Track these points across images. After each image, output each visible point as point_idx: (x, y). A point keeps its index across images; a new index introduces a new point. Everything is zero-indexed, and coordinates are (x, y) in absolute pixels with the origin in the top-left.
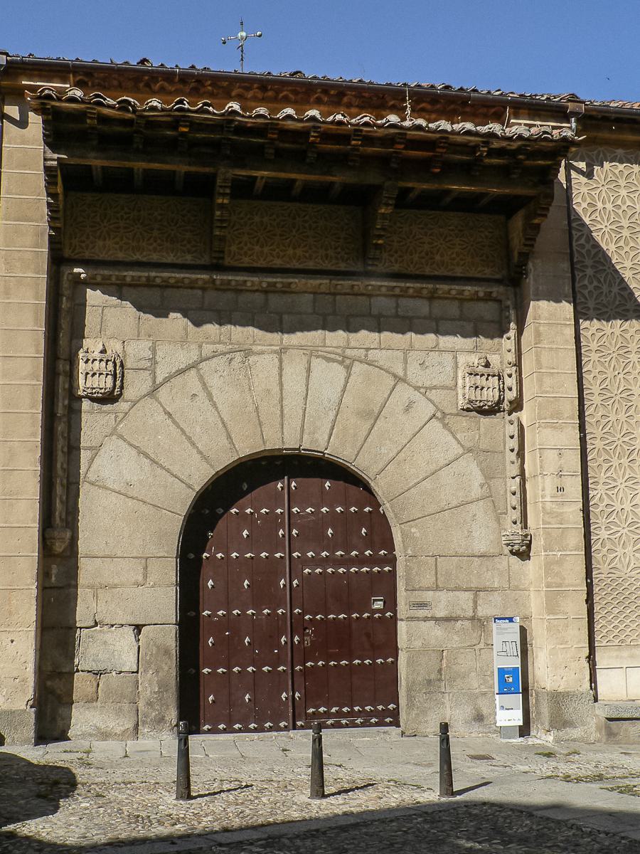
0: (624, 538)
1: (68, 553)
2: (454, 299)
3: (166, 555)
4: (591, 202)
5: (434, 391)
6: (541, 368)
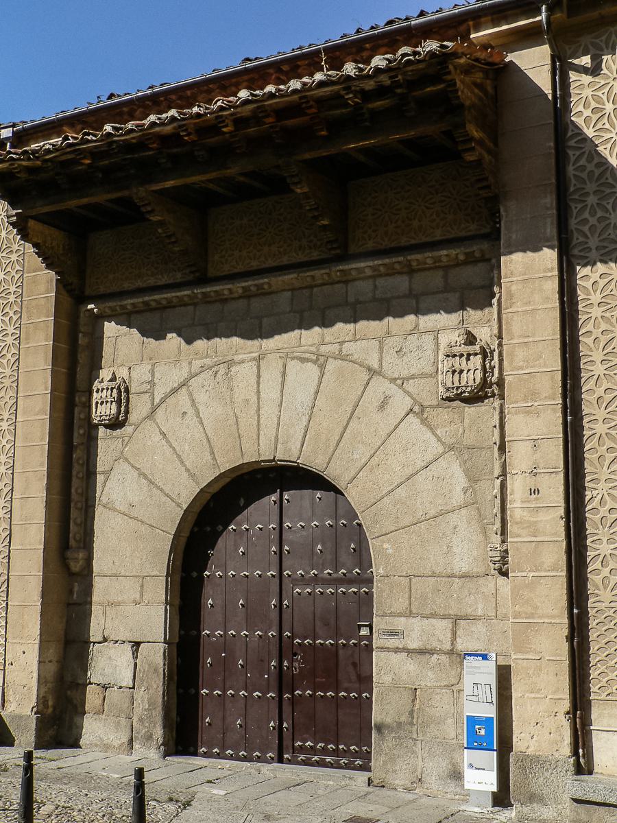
1: (86, 572)
3: (158, 574)
4: (598, 106)
6: (512, 339)
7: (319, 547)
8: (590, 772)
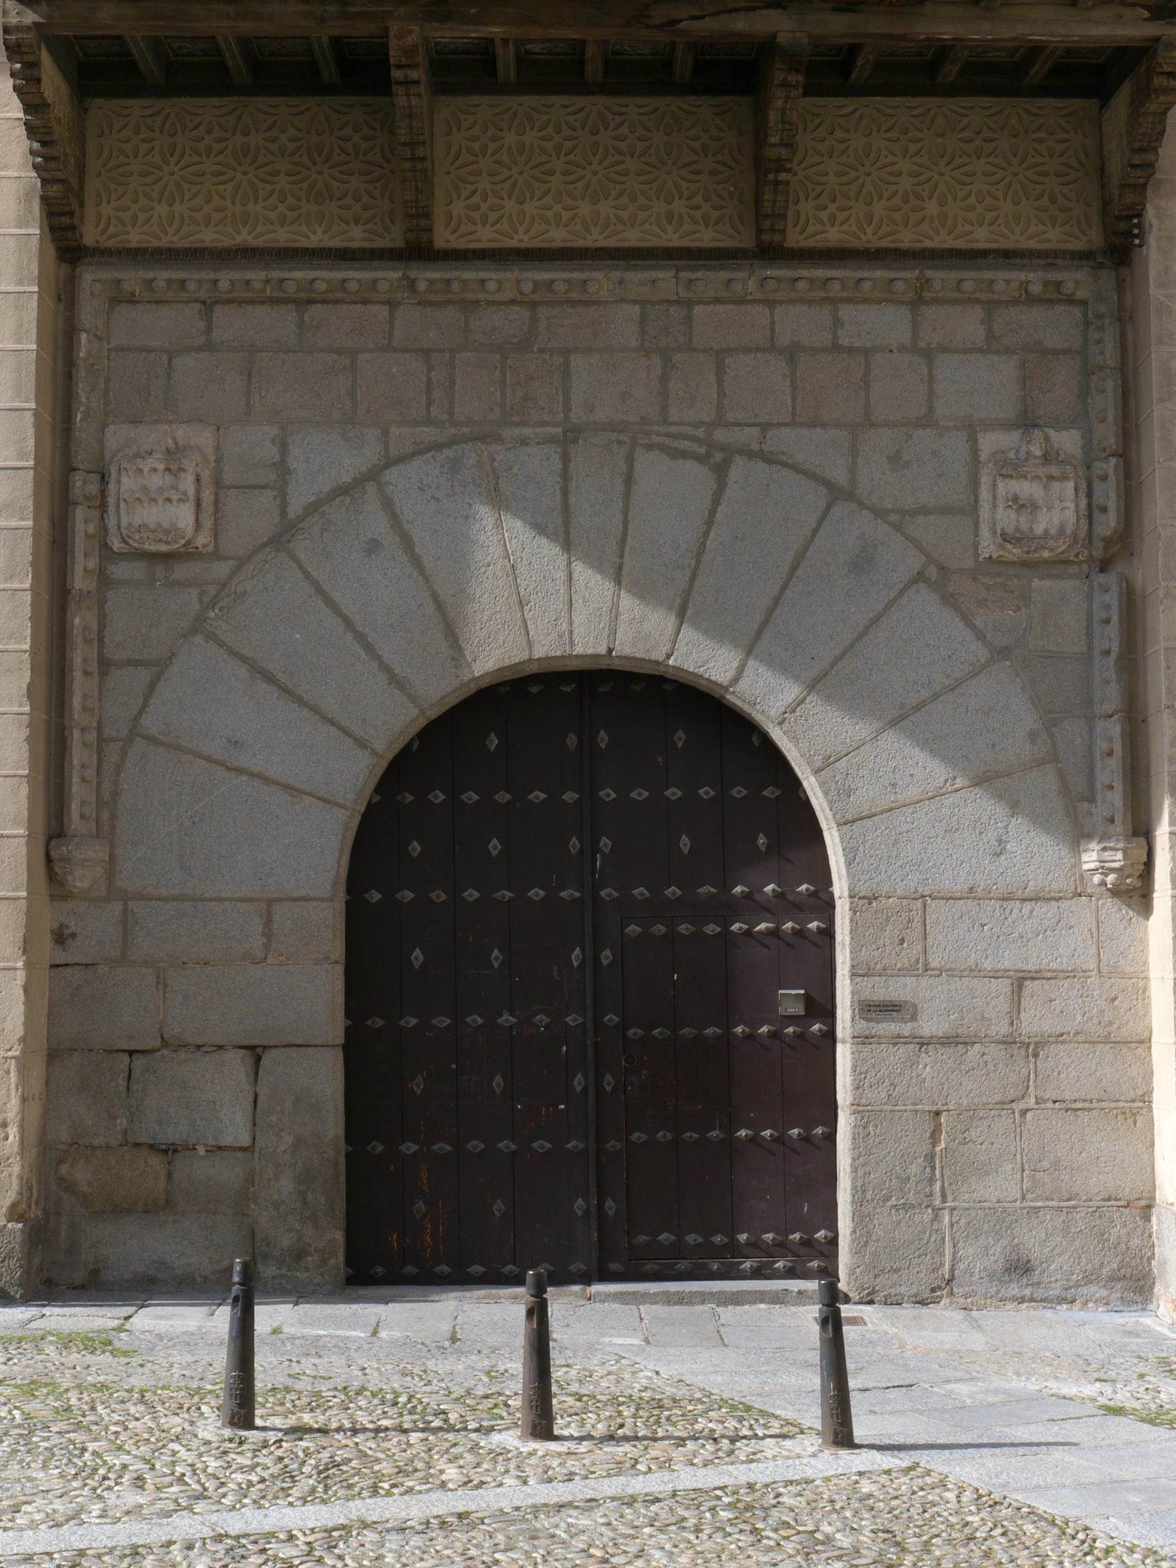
2: (972, 301)
5: (920, 519)
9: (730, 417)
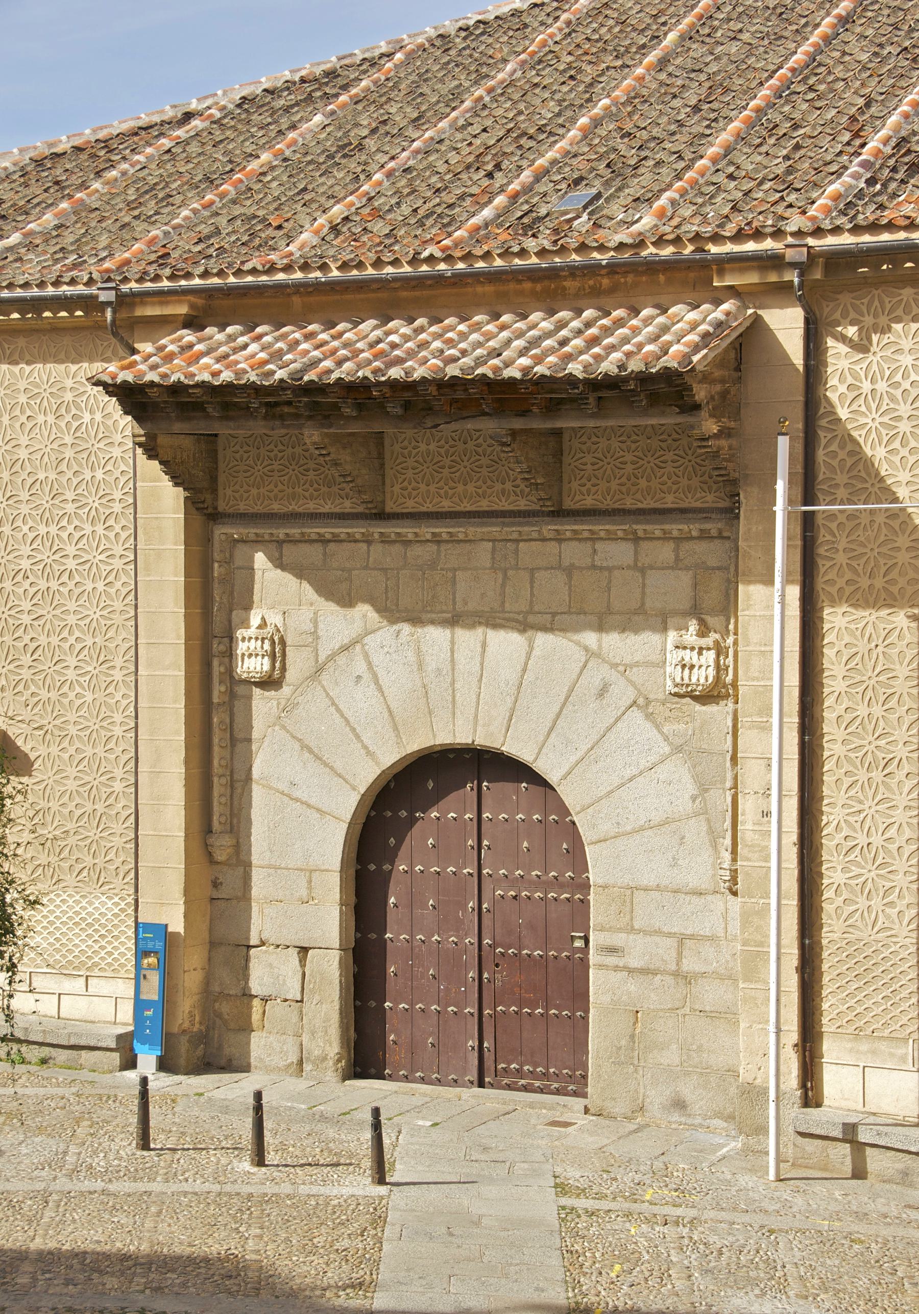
0: (869, 885)
4: (854, 382)
7: (525, 844)
8: (819, 1105)
9: (536, 608)
